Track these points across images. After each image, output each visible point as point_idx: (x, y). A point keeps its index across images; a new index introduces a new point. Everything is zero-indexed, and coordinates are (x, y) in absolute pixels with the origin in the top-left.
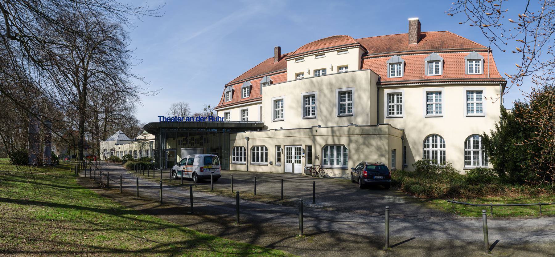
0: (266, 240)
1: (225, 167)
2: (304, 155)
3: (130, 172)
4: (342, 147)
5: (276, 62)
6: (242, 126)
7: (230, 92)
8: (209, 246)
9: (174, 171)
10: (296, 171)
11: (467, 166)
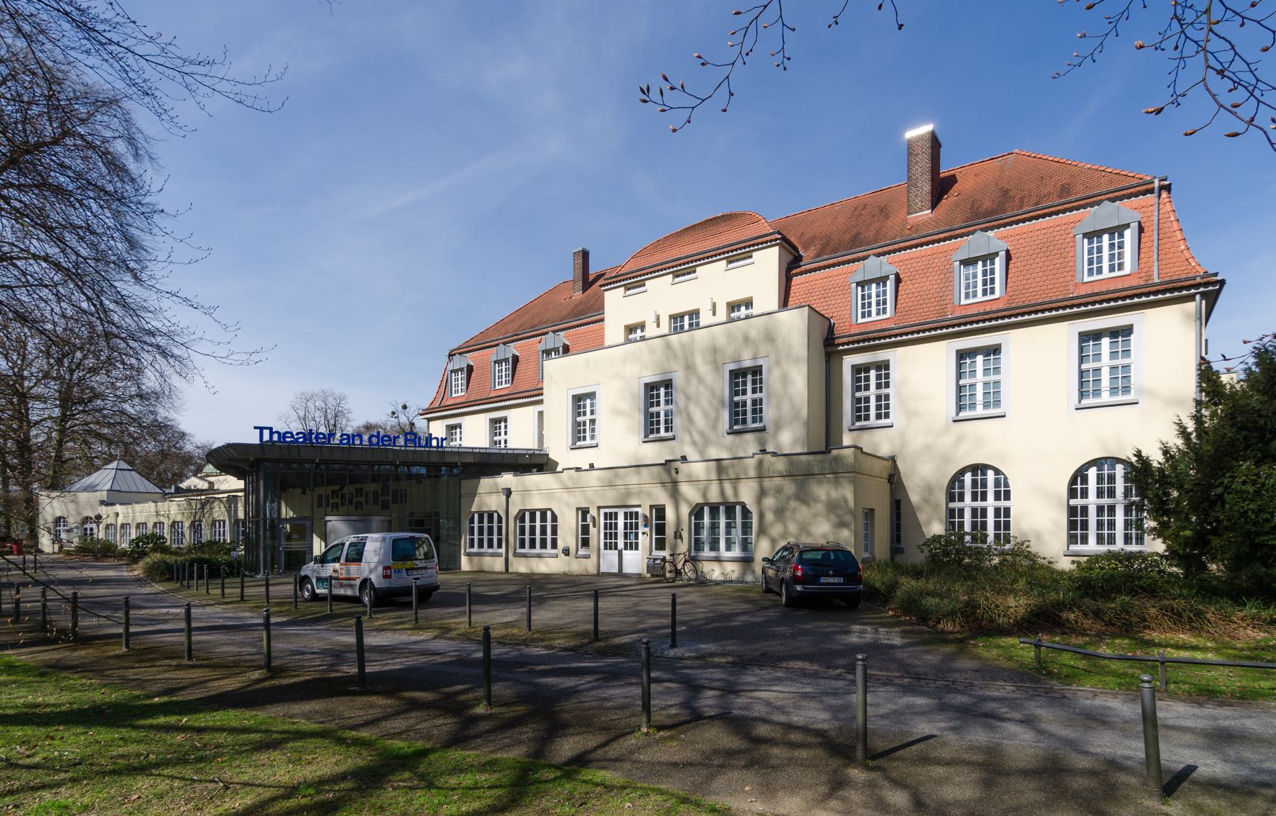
0: (567, 747)
1: (450, 564)
2: (647, 530)
3: (158, 587)
4: (738, 508)
5: (578, 295)
6: (492, 460)
7: (461, 370)
8: (422, 777)
9: (306, 579)
10: (628, 569)
11: (1073, 548)
